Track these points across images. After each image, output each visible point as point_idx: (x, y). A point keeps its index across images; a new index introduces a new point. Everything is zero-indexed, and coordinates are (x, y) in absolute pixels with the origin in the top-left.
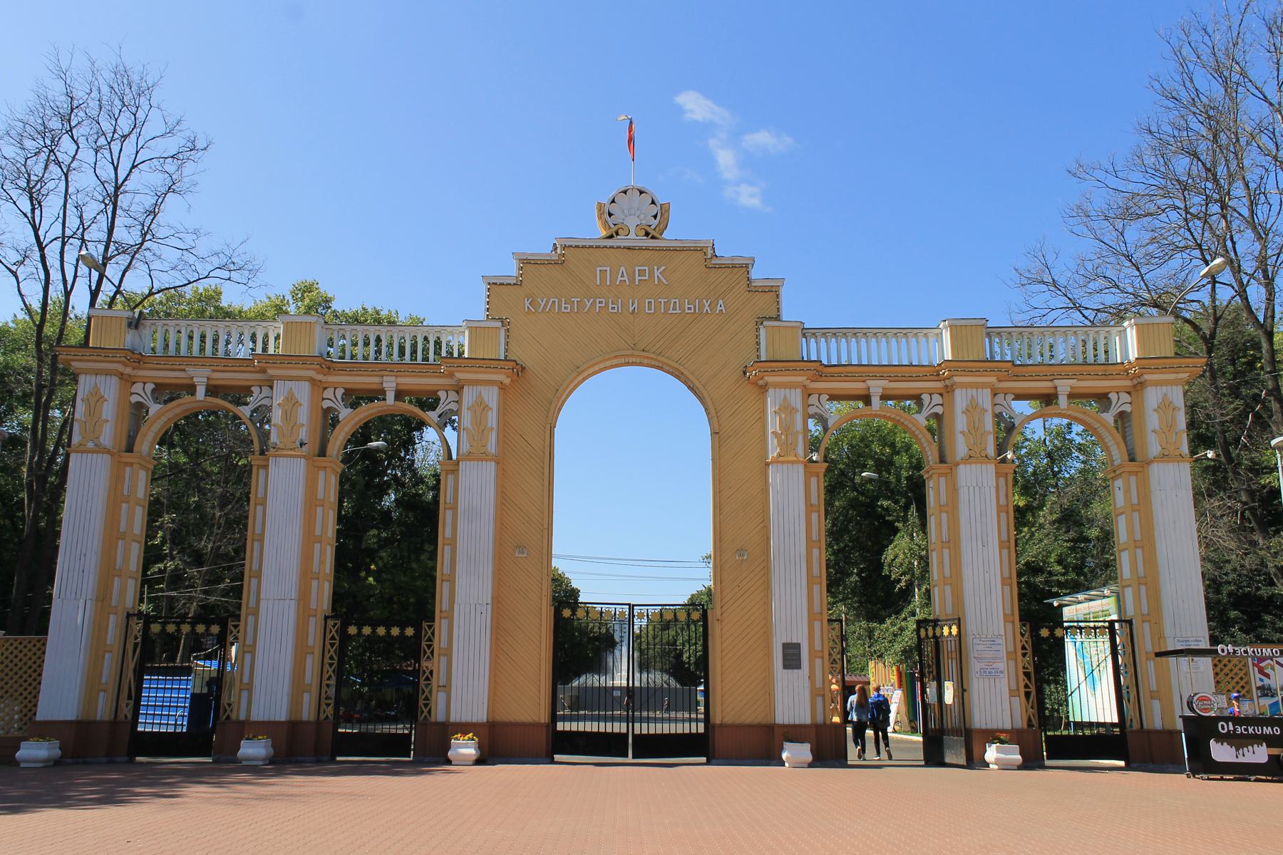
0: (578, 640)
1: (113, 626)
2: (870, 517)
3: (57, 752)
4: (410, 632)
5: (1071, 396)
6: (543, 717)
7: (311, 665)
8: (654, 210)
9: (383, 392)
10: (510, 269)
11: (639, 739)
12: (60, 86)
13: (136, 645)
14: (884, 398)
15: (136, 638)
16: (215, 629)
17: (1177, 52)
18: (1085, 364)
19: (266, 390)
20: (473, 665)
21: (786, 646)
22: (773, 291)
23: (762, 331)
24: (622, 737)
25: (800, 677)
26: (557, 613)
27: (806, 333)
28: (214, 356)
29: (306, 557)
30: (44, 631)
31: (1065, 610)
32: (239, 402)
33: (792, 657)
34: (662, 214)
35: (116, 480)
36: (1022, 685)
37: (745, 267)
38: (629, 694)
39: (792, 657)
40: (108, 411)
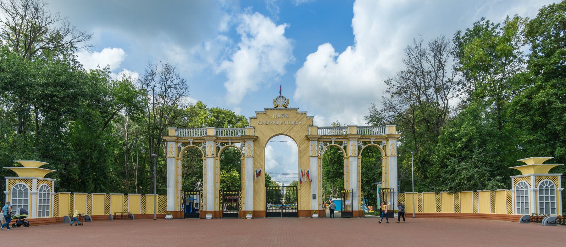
0: (273, 195)
1: (218, 192)
7: (218, 199)
10: (255, 115)
11: (540, 200)
12: (150, 70)
16: (225, 193)
18: (183, 137)
20: (251, 199)
22: (311, 118)
24: (280, 213)
25: (316, 201)
27: (318, 128)
31: (378, 185)
32: (341, 145)
33: (314, 197)
34: (287, 102)
35: (176, 164)
37: (306, 113)
39: (314, 197)
40: (174, 149)
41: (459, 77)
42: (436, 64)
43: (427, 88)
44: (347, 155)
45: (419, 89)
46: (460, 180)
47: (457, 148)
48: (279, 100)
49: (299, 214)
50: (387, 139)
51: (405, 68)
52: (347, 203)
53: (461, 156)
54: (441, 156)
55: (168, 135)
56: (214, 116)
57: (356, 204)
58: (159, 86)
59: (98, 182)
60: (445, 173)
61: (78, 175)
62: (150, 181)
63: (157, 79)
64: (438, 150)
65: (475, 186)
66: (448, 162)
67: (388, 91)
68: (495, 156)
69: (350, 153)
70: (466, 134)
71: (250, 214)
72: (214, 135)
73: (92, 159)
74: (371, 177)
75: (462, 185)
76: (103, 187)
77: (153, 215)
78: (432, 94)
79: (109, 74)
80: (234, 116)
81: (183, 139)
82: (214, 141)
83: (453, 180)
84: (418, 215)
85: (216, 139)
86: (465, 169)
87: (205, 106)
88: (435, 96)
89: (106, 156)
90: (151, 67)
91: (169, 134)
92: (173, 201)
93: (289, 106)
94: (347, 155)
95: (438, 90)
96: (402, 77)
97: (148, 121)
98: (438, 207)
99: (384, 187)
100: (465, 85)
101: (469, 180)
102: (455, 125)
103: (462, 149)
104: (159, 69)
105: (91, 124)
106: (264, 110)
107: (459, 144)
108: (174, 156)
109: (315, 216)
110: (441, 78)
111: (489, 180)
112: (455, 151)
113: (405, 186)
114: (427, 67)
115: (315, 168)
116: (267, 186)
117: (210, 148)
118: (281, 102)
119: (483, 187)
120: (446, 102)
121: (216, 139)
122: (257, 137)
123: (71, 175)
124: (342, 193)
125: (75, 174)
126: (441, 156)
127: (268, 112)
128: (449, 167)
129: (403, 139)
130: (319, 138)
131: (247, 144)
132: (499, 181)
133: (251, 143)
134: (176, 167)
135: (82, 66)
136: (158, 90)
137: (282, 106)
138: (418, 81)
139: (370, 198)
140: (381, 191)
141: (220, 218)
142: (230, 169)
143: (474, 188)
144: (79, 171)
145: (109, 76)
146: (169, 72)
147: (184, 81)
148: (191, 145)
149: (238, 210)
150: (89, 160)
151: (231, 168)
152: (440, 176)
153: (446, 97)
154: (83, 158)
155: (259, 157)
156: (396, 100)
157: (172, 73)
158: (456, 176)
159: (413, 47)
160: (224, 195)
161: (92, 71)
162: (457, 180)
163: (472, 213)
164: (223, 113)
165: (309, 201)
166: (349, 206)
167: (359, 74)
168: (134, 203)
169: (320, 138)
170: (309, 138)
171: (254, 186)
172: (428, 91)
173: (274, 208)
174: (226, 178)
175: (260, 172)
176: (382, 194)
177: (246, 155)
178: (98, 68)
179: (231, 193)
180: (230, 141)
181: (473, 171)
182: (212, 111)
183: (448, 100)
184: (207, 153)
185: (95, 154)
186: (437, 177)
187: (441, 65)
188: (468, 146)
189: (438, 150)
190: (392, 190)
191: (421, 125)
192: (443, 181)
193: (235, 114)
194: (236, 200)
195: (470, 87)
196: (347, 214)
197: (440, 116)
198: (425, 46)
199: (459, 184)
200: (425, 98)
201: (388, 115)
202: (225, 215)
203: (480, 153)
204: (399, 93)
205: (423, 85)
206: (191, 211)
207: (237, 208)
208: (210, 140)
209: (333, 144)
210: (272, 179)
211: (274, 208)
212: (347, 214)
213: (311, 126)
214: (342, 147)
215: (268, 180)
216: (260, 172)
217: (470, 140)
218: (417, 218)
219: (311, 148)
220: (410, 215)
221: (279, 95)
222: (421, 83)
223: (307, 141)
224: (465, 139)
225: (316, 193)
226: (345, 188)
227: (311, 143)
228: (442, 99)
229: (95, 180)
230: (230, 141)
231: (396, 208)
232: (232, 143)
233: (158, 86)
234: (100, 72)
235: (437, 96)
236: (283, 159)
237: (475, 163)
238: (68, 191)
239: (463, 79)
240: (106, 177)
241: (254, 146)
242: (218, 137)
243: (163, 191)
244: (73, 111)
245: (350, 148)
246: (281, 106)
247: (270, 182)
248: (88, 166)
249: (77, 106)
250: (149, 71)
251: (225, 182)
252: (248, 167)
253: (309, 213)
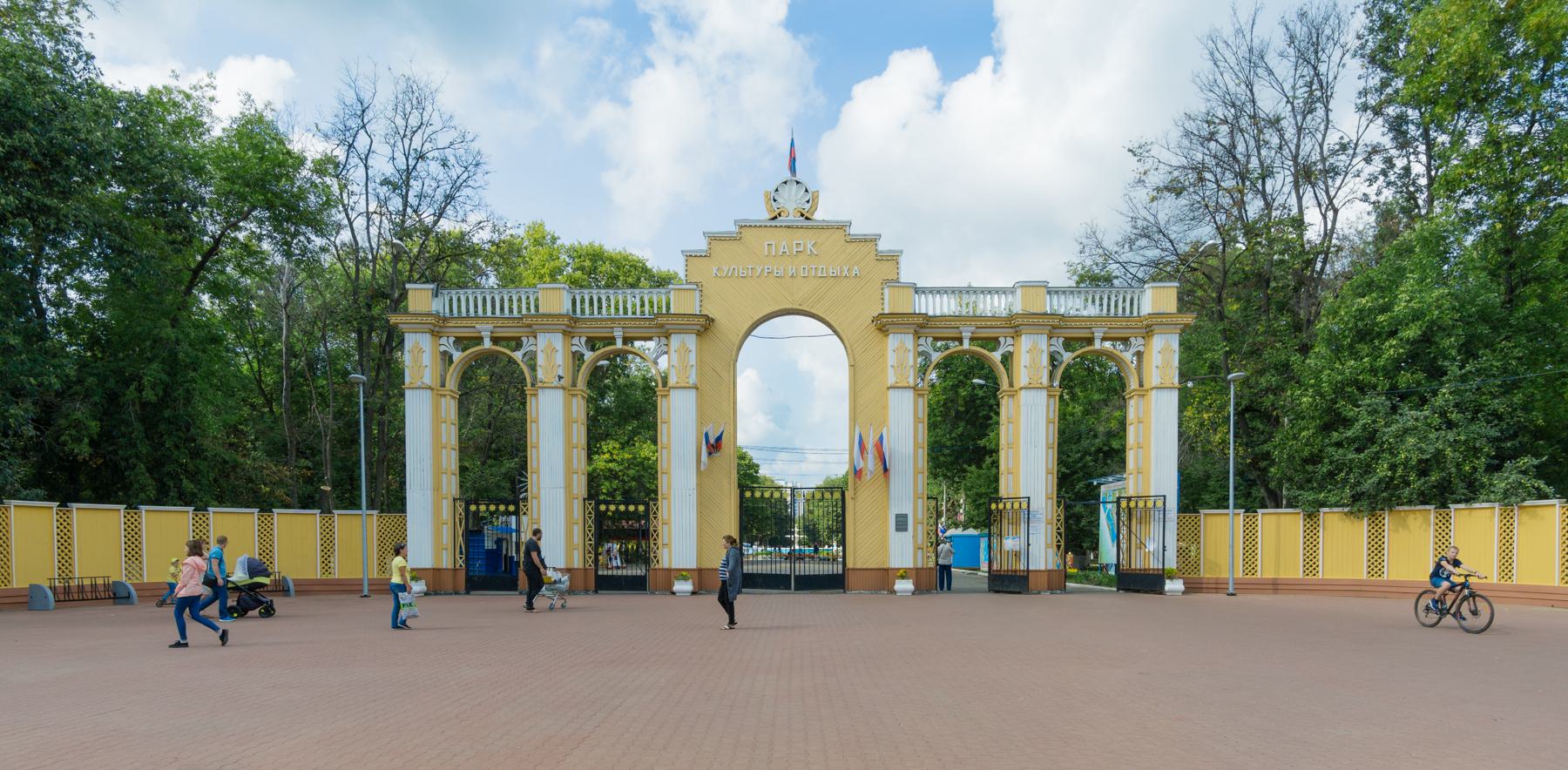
0: (762, 515)
1: (446, 506)
2: (963, 430)
3: (424, 588)
4: (641, 508)
5: (972, 339)
8: (809, 196)
9: (614, 339)
10: (701, 245)
11: (798, 578)
14: (1104, 339)
17: (1212, 54)
18: (460, 317)
19: (532, 340)
20: (687, 530)
21: (898, 516)
22: (893, 258)
23: (886, 291)
26: (742, 496)
27: (917, 290)
28: (468, 317)
29: (436, 434)
30: (404, 511)
32: (993, 350)
34: (813, 201)
35: (436, 409)
37: (873, 240)
38: (781, 544)
40: (426, 359)
41: (1377, 133)
42: (1302, 92)
43: (1266, 173)
44: (1011, 385)
45: (1242, 176)
46: (1393, 467)
47: (1381, 362)
48: (785, 191)
49: (851, 579)
50: (1148, 331)
51: (1198, 105)
52: (1009, 544)
53: (1394, 388)
54: (1325, 387)
55: (406, 312)
56: (582, 269)
57: (1038, 547)
58: (387, 150)
59: (169, 468)
60: (1339, 445)
61: (92, 443)
62: (355, 469)
63: (378, 127)
64: (1317, 374)
65: (1444, 489)
66: (1349, 411)
67: (1140, 181)
68: (1507, 390)
69: (1022, 378)
70: (1417, 316)
71: (685, 579)
72: (564, 311)
73: (140, 390)
74: (1088, 458)
75: (1397, 487)
76: (188, 485)
77: (359, 583)
78: (1286, 189)
79: (213, 106)
80: (645, 270)
81: (464, 323)
82: (565, 333)
83: (1368, 469)
84: (1243, 587)
85: (570, 325)
86: (1413, 434)
87: (554, 239)
88: (1293, 200)
89: (193, 380)
90: (353, 84)
91: (411, 309)
92: (429, 530)
93: (819, 215)
94: (1011, 385)
95: (1305, 175)
96: (1188, 134)
97: (353, 271)
98: (1310, 563)
99: (1131, 493)
100: (1389, 162)
101: (1423, 469)
102: (1370, 286)
103: (1397, 366)
104: (383, 99)
105: (129, 266)
106: (733, 229)
107: (1391, 349)
108: (427, 380)
109: (904, 586)
110: (1319, 137)
111: (1493, 468)
112: (1373, 371)
113: (1197, 493)
114: (1269, 101)
115: (905, 427)
116: (742, 488)
117: (550, 355)
118: (791, 201)
119: (1472, 492)
120: (1330, 214)
121: (570, 325)
122: (710, 321)
123: (64, 444)
124: (988, 513)
125: (79, 440)
126: (1325, 387)
127: (747, 233)
128: (1358, 426)
129: (1430, 145)
130: (922, 325)
131: (675, 341)
132: (1524, 473)
133: (691, 341)
134: (437, 420)
135: (90, 57)
136: (382, 166)
137: (792, 215)
138: (1241, 148)
139: (1077, 536)
140: (1124, 504)
141: (586, 591)
142: (631, 439)
143: (1441, 496)
144: (94, 426)
145: (210, 113)
146: (420, 105)
147: (469, 137)
148: (487, 344)
149: (647, 561)
150: (131, 393)
151: (635, 432)
152: (1315, 459)
153: (1331, 201)
154: (111, 383)
155: (716, 388)
156: (1169, 207)
157: (429, 109)
158: (1376, 457)
159: (1228, 32)
160: (600, 518)
161: (152, 90)
162: (1382, 470)
163: (1364, 576)
164: (612, 260)
165: (890, 532)
166: (1017, 554)
167: (1033, 158)
168: (296, 540)
169: (922, 326)
170: (885, 324)
171: (699, 485)
172: (1269, 182)
173: (758, 556)
174: (621, 463)
175: (719, 439)
176: (1124, 518)
177: (672, 381)
178: (172, 83)
179: (632, 508)
180: (618, 333)
181: (1439, 441)
182: (575, 253)
183: (1336, 211)
184: (540, 374)
185: (153, 372)
186: (1306, 461)
187: (1318, 95)
188: (1424, 356)
189: (1317, 374)
190: (1160, 504)
191: (1247, 298)
192: (1331, 474)
193: (649, 265)
194: (645, 534)
195: (1407, 169)
196: (1009, 582)
197: (1310, 263)
198: (1270, 33)
199: (1387, 484)
200: (1262, 203)
201: (1139, 259)
202: (606, 584)
203: (1464, 379)
204: (1176, 189)
205: (1254, 162)
206: (494, 565)
207: (642, 557)
208: (549, 330)
209: (966, 345)
210: (763, 472)
211: (758, 556)
212: (1009, 582)
213: (894, 282)
214: (996, 356)
215: (747, 476)
216: (719, 439)
217: (1426, 339)
218: (1240, 597)
219: (891, 358)
220: (1218, 586)
221: (787, 175)
222: (1249, 156)
223: (881, 335)
224: (1412, 332)
225: (907, 509)
226: (1003, 492)
227: (893, 341)
228: (1320, 205)
229: (155, 467)
230: (618, 333)
231: (1172, 563)
232: (626, 340)
233: (382, 149)
234: (179, 98)
235: (1300, 199)
236: (801, 404)
237: (1443, 414)
238: (50, 498)
239: (1387, 141)
240: (197, 453)
241: (700, 351)
242: (576, 320)
243: (393, 501)
244: (46, 210)
245: (1022, 360)
246: (792, 217)
247: (755, 479)
248: (132, 413)
249: (65, 195)
250: (350, 97)
251: (616, 477)
252: (679, 420)
253: (883, 579)
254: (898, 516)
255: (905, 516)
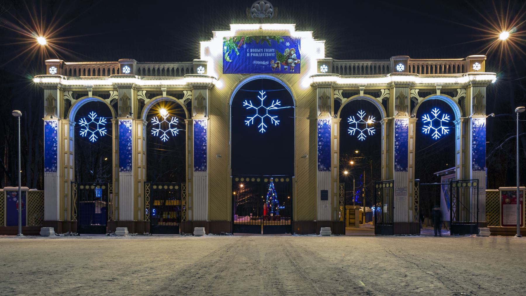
6: (229, 219)
13: (75, 194)
15: (75, 191)
21: (327, 199)
36: (414, 206)
140: (454, 185)
225: (328, 188)
254: (327, 199)
255: (327, 191)
